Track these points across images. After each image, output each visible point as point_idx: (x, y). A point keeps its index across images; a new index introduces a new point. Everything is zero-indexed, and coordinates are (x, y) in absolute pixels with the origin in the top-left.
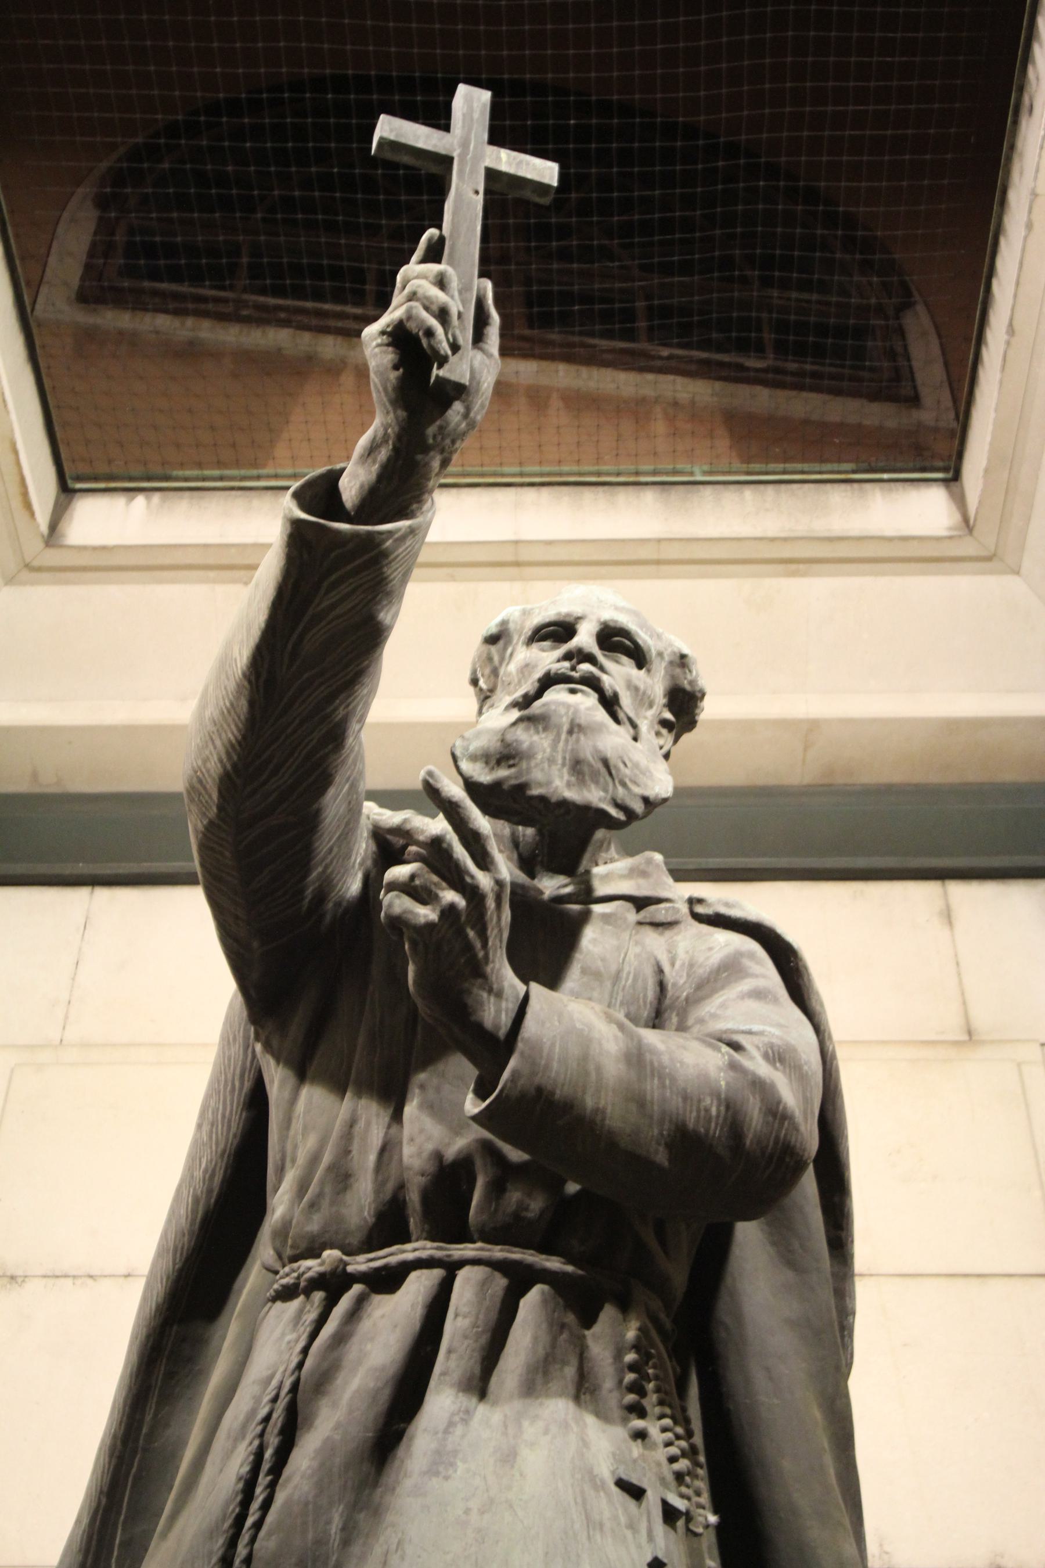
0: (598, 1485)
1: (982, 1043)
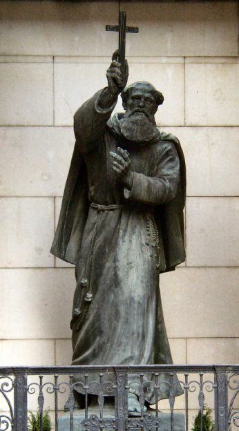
0: (142, 245)
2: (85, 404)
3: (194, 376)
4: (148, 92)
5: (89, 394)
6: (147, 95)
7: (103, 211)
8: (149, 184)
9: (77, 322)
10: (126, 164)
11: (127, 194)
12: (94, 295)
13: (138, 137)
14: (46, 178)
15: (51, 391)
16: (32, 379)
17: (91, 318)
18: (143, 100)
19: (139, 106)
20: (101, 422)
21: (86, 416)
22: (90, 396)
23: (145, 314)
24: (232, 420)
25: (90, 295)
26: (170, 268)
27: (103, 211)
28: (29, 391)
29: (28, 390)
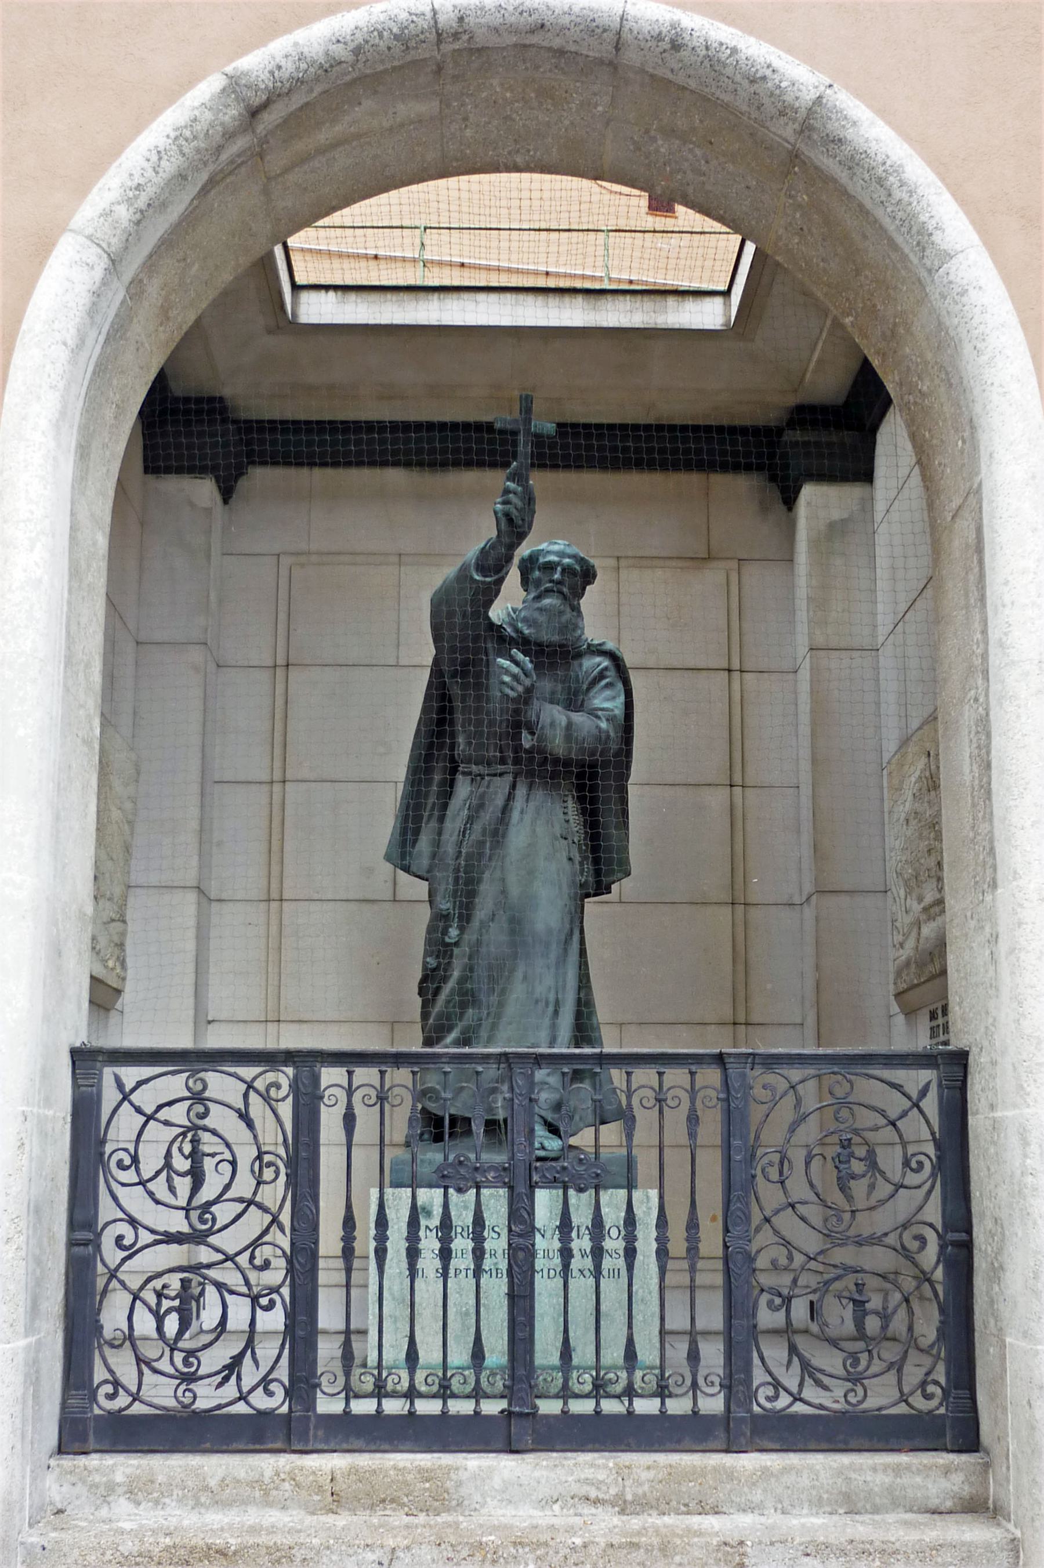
1: (714, 558)
2: (442, 1133)
3: (645, 1076)
4: (569, 557)
5: (451, 1115)
6: (567, 561)
7: (482, 776)
8: (569, 725)
9: (430, 983)
10: (528, 682)
11: (527, 741)
12: (462, 929)
13: (549, 636)
14: (382, 750)
15: (372, 1102)
16: (331, 1076)
17: (456, 974)
18: (559, 569)
19: (552, 581)
20: (476, 1169)
21: (446, 1158)
22: (453, 1120)
23: (562, 960)
24: (759, 1168)
25: (454, 932)
26: (601, 888)
27: (482, 776)
28: (326, 1100)
29: (322, 1098)
